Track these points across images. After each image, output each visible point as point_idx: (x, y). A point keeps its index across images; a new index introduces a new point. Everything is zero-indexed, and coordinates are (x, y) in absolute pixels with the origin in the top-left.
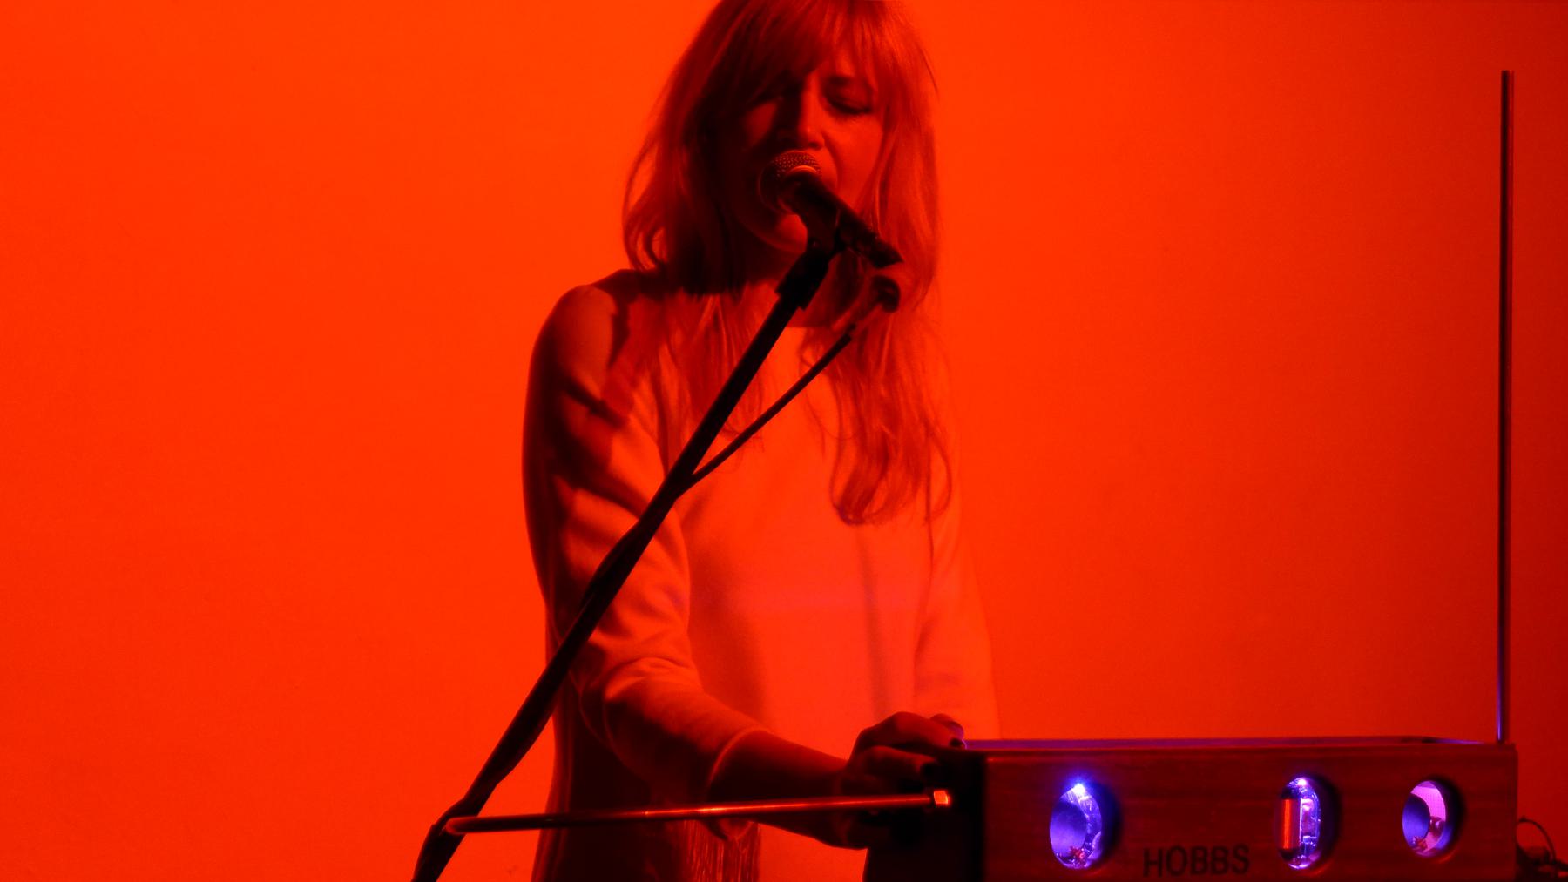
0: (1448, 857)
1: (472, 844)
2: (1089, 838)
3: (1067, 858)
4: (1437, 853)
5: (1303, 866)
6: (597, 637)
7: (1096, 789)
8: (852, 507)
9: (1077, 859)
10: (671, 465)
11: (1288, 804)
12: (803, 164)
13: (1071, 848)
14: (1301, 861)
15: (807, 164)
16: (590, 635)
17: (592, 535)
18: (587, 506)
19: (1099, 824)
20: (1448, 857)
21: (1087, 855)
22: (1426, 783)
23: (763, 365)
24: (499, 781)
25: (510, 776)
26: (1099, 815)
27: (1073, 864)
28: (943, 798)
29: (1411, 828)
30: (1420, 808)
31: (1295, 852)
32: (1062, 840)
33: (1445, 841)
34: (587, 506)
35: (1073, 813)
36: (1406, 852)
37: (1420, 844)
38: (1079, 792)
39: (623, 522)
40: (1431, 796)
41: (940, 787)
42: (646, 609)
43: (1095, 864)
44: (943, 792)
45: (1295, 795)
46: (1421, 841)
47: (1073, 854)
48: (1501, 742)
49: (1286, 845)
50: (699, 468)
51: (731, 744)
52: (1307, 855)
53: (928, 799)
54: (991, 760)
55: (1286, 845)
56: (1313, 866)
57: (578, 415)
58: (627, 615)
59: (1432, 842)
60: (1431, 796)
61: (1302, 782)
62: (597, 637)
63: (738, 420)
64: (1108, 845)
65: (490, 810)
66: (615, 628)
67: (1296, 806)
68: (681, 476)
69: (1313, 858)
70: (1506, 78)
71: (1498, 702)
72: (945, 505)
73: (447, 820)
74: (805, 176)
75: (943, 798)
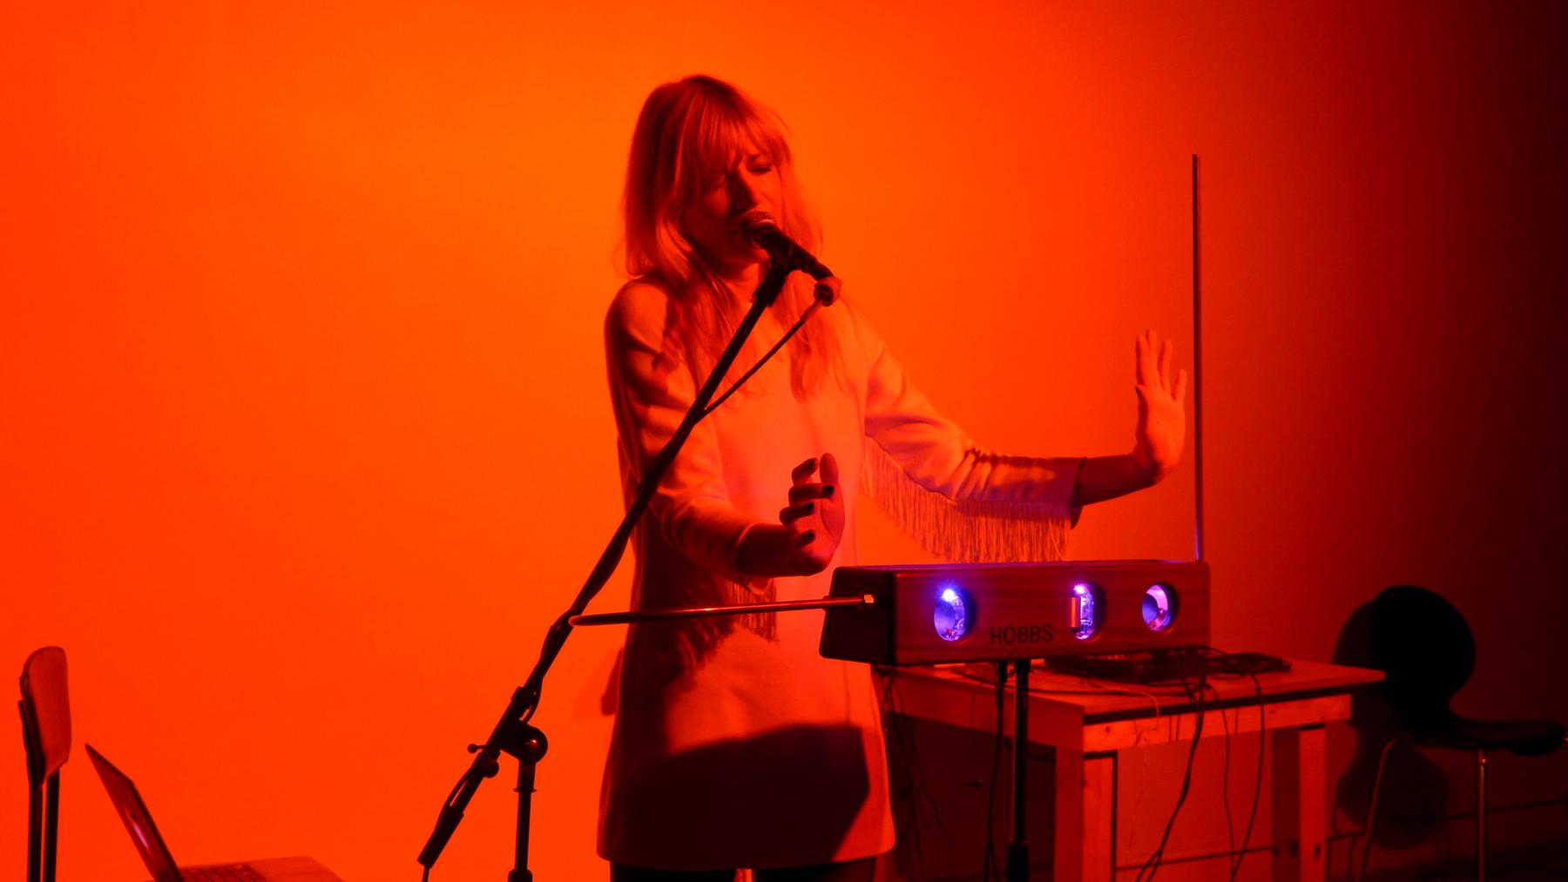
0: (1170, 631)
1: (578, 633)
2: (956, 622)
3: (944, 635)
5: (1085, 637)
6: (662, 490)
7: (965, 595)
8: (799, 386)
9: (950, 635)
10: (701, 387)
17: (658, 431)
18: (658, 415)
19: (963, 613)
20: (1170, 631)
22: (1156, 586)
26: (963, 609)
27: (948, 638)
28: (869, 599)
29: (1147, 614)
30: (1152, 602)
31: (1080, 628)
32: (941, 624)
33: (1169, 618)
34: (658, 415)
35: (948, 610)
36: (1144, 628)
38: (950, 596)
39: (675, 420)
40: (1159, 594)
41: (868, 593)
42: (694, 469)
43: (962, 637)
44: (870, 596)
45: (1078, 597)
47: (948, 633)
48: (1198, 562)
49: (1073, 626)
50: (706, 408)
51: (747, 530)
52: (1086, 631)
53: (860, 600)
54: (899, 575)
56: (1091, 637)
57: (645, 366)
58: (683, 474)
59: (1159, 623)
60: (1159, 594)
62: (662, 490)
63: (738, 368)
64: (969, 625)
65: (591, 609)
66: (673, 482)
67: (1079, 602)
68: (697, 413)
69: (1090, 632)
70: (1195, 158)
71: (1196, 537)
72: (944, 532)
73: (570, 616)
75: (869, 599)
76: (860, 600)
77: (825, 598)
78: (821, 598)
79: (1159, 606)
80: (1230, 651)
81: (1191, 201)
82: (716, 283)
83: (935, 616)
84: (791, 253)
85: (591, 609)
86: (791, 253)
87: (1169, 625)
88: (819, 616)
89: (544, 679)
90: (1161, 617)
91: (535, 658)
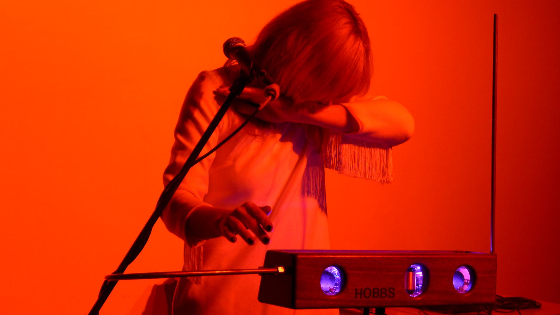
1: (121, 284)
4: (467, 292)
9: (332, 292)
11: (411, 273)
12: (240, 43)
13: (330, 288)
14: (415, 294)
15: (241, 43)
16: (175, 191)
21: (335, 290)
23: (185, 177)
24: (128, 265)
25: (133, 263)
28: (281, 270)
29: (456, 283)
30: (461, 276)
37: (460, 289)
40: (465, 273)
42: (346, 23)
45: (414, 271)
46: (461, 288)
47: (330, 290)
49: (411, 288)
53: (276, 270)
55: (411, 288)
56: (419, 296)
59: (467, 288)
60: (465, 273)
61: (412, 266)
65: (128, 271)
67: (414, 275)
71: (491, 239)
74: (240, 47)
75: (281, 270)
76: (276, 270)
77: (260, 268)
78: (257, 268)
79: (465, 278)
80: (504, 296)
81: (491, 123)
82: (331, 164)
83: (453, 278)
84: (251, 67)
85: (128, 271)
86: (251, 67)
87: (471, 290)
88: (257, 279)
89: (100, 311)
90: (467, 284)
91: (95, 298)
